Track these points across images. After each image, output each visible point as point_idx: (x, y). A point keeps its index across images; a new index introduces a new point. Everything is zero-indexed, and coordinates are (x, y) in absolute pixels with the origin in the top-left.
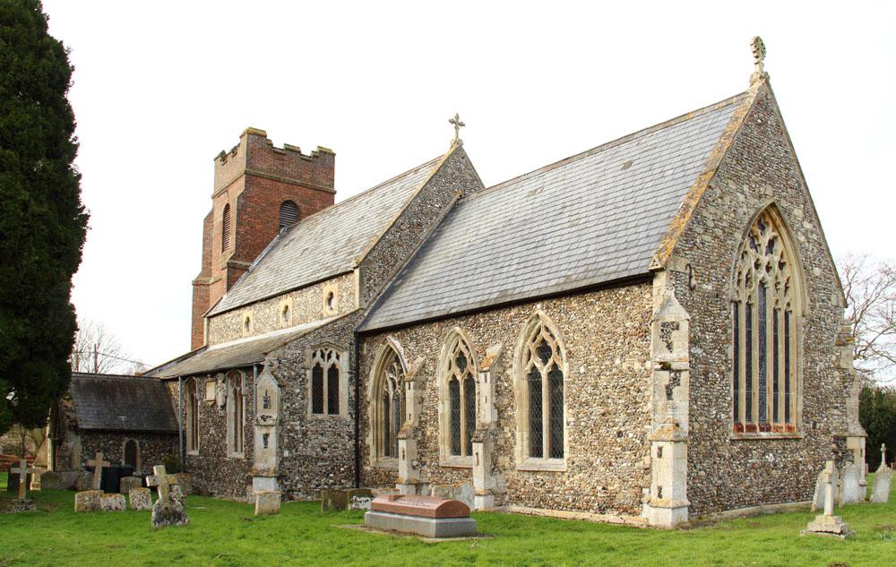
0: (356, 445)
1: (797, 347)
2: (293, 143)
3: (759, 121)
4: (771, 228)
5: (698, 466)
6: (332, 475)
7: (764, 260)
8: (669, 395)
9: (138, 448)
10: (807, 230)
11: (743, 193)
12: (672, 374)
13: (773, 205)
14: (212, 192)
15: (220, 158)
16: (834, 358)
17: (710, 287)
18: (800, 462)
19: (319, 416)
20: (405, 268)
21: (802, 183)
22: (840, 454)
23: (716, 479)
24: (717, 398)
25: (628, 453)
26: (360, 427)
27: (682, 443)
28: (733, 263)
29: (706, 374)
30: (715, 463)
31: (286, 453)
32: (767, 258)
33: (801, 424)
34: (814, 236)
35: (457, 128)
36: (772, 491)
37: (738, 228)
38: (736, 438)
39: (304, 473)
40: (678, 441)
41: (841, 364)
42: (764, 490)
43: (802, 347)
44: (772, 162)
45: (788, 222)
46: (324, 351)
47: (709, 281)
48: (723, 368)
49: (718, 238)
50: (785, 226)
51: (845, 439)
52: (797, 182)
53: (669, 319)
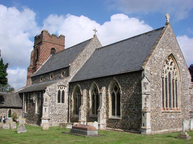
7: (170, 67)
8: (146, 100)
13: (172, 54)
19: (59, 103)
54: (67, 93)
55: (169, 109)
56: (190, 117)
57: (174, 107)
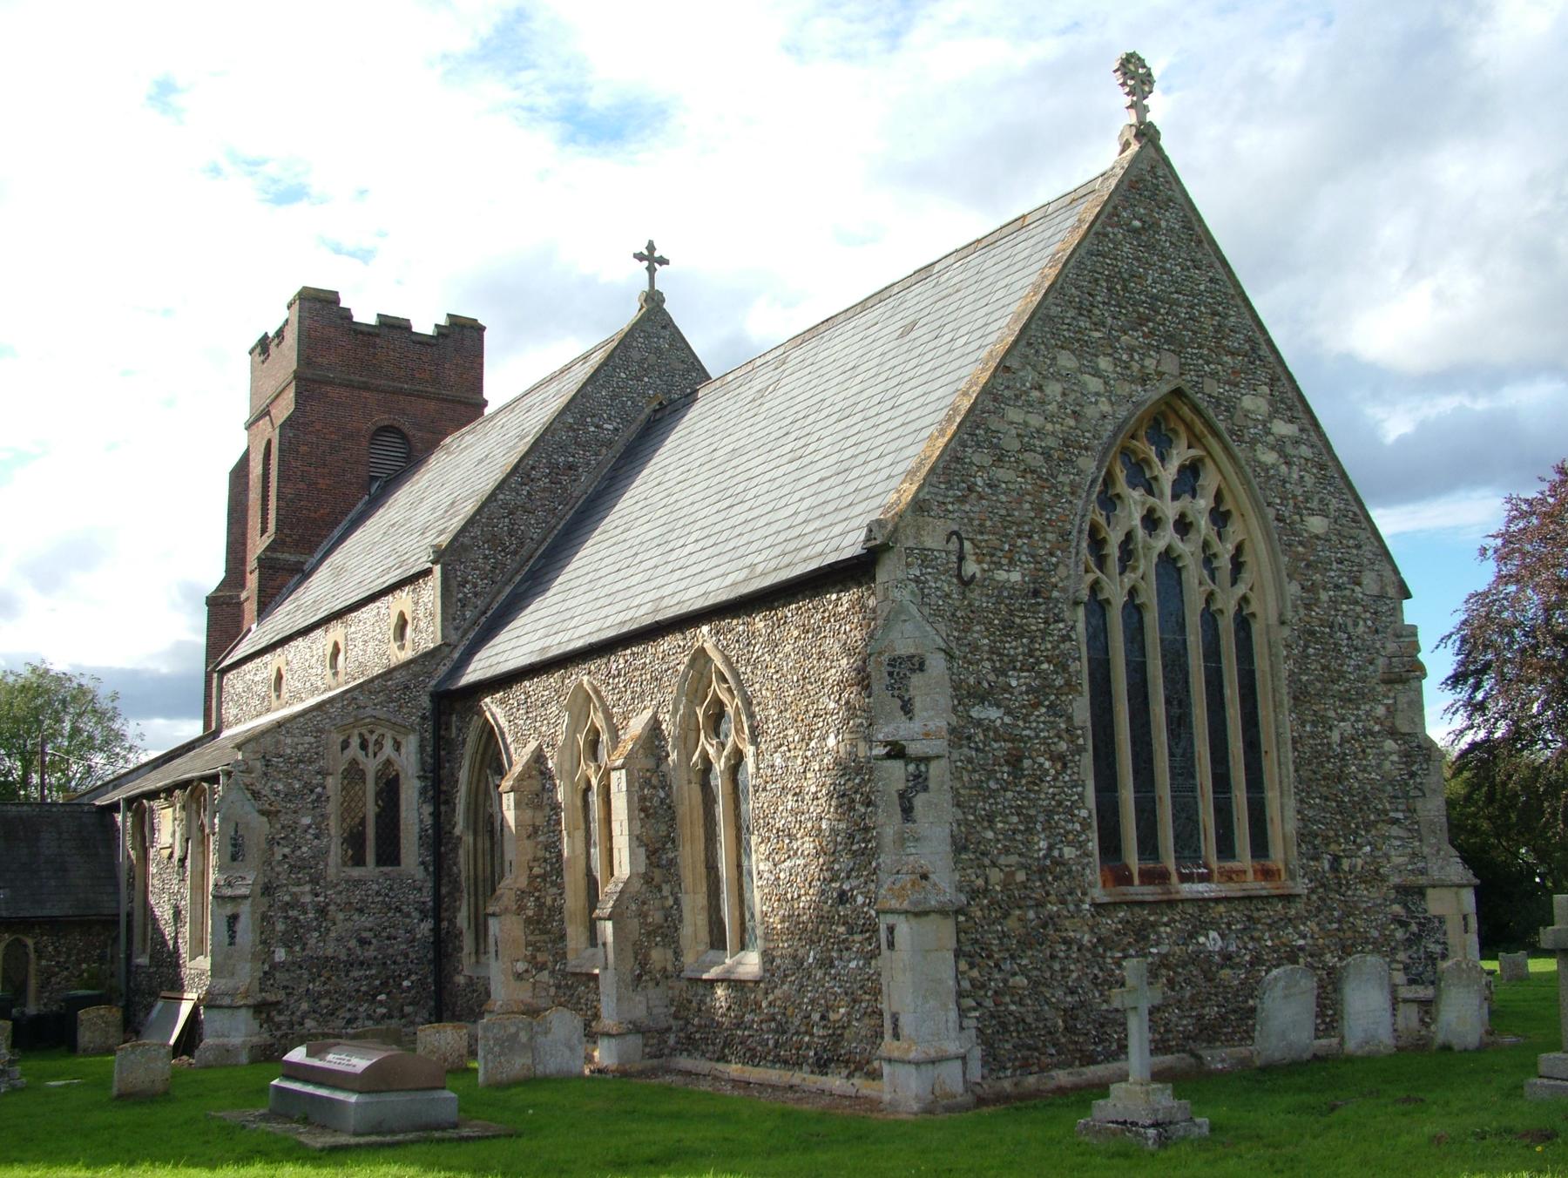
0: (436, 930)
1: (1274, 690)
2: (395, 311)
3: (1137, 223)
4: (1184, 442)
5: (1007, 966)
6: (382, 997)
7: (1169, 510)
8: (907, 811)
9: (32, 956)
10: (1281, 440)
11: (1097, 373)
12: (911, 768)
13: (1178, 393)
14: (245, 414)
15: (258, 350)
16: (1380, 711)
17: (1015, 576)
18: (1301, 948)
19: (356, 873)
20: (540, 557)
21: (1261, 340)
22: (1414, 928)
23: (1060, 993)
24: (1050, 813)
25: (858, 938)
26: (444, 890)
27: (933, 916)
28: (1077, 522)
29: (1015, 761)
30: (1053, 957)
31: (280, 955)
32: (1178, 505)
33: (1295, 863)
34: (1305, 450)
35: (651, 271)
36: (1223, 1018)
37: (1087, 449)
38: (1106, 900)
39: (320, 996)
40: (926, 913)
41: (1398, 723)
42: (1200, 1017)
43: (1285, 690)
44: (1177, 303)
45: (1222, 426)
46: (367, 736)
47: (1011, 562)
48: (1063, 746)
49: (1033, 472)
50: (1215, 433)
51: (1421, 892)
52: (1249, 340)
53: (904, 648)
54: (417, 784)
55: (1174, 878)
56: (1400, 934)
57: (1226, 848)
